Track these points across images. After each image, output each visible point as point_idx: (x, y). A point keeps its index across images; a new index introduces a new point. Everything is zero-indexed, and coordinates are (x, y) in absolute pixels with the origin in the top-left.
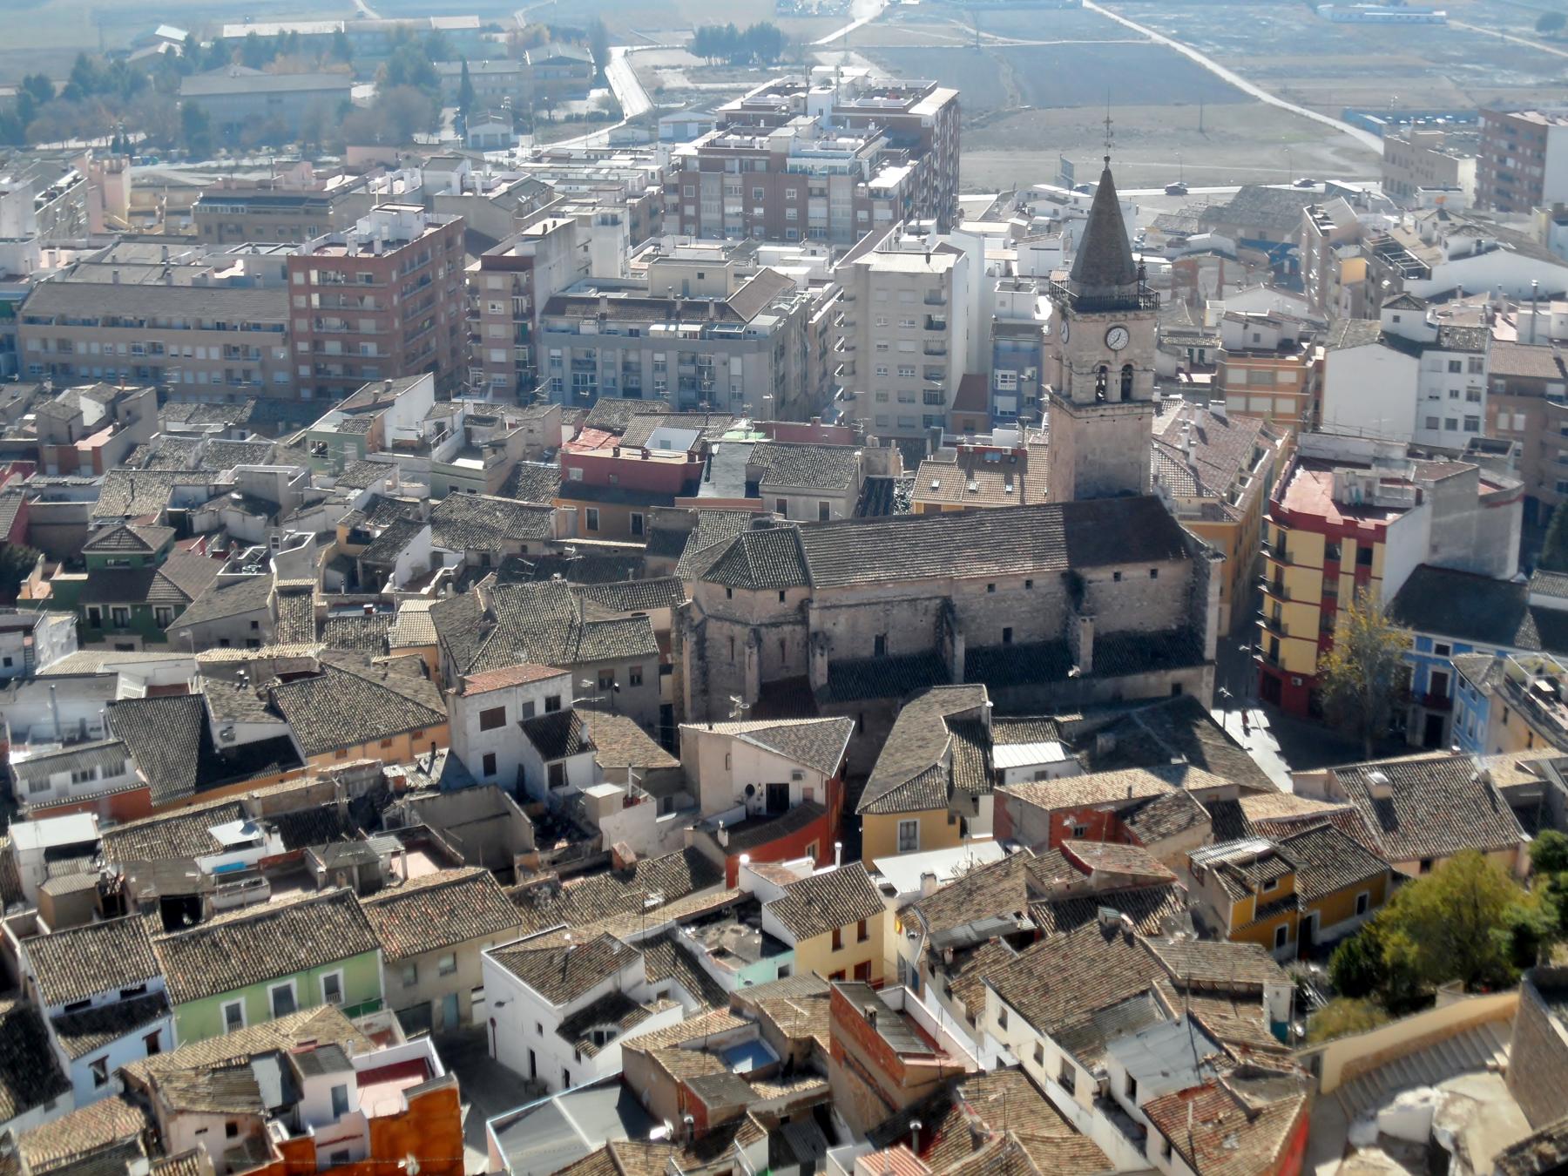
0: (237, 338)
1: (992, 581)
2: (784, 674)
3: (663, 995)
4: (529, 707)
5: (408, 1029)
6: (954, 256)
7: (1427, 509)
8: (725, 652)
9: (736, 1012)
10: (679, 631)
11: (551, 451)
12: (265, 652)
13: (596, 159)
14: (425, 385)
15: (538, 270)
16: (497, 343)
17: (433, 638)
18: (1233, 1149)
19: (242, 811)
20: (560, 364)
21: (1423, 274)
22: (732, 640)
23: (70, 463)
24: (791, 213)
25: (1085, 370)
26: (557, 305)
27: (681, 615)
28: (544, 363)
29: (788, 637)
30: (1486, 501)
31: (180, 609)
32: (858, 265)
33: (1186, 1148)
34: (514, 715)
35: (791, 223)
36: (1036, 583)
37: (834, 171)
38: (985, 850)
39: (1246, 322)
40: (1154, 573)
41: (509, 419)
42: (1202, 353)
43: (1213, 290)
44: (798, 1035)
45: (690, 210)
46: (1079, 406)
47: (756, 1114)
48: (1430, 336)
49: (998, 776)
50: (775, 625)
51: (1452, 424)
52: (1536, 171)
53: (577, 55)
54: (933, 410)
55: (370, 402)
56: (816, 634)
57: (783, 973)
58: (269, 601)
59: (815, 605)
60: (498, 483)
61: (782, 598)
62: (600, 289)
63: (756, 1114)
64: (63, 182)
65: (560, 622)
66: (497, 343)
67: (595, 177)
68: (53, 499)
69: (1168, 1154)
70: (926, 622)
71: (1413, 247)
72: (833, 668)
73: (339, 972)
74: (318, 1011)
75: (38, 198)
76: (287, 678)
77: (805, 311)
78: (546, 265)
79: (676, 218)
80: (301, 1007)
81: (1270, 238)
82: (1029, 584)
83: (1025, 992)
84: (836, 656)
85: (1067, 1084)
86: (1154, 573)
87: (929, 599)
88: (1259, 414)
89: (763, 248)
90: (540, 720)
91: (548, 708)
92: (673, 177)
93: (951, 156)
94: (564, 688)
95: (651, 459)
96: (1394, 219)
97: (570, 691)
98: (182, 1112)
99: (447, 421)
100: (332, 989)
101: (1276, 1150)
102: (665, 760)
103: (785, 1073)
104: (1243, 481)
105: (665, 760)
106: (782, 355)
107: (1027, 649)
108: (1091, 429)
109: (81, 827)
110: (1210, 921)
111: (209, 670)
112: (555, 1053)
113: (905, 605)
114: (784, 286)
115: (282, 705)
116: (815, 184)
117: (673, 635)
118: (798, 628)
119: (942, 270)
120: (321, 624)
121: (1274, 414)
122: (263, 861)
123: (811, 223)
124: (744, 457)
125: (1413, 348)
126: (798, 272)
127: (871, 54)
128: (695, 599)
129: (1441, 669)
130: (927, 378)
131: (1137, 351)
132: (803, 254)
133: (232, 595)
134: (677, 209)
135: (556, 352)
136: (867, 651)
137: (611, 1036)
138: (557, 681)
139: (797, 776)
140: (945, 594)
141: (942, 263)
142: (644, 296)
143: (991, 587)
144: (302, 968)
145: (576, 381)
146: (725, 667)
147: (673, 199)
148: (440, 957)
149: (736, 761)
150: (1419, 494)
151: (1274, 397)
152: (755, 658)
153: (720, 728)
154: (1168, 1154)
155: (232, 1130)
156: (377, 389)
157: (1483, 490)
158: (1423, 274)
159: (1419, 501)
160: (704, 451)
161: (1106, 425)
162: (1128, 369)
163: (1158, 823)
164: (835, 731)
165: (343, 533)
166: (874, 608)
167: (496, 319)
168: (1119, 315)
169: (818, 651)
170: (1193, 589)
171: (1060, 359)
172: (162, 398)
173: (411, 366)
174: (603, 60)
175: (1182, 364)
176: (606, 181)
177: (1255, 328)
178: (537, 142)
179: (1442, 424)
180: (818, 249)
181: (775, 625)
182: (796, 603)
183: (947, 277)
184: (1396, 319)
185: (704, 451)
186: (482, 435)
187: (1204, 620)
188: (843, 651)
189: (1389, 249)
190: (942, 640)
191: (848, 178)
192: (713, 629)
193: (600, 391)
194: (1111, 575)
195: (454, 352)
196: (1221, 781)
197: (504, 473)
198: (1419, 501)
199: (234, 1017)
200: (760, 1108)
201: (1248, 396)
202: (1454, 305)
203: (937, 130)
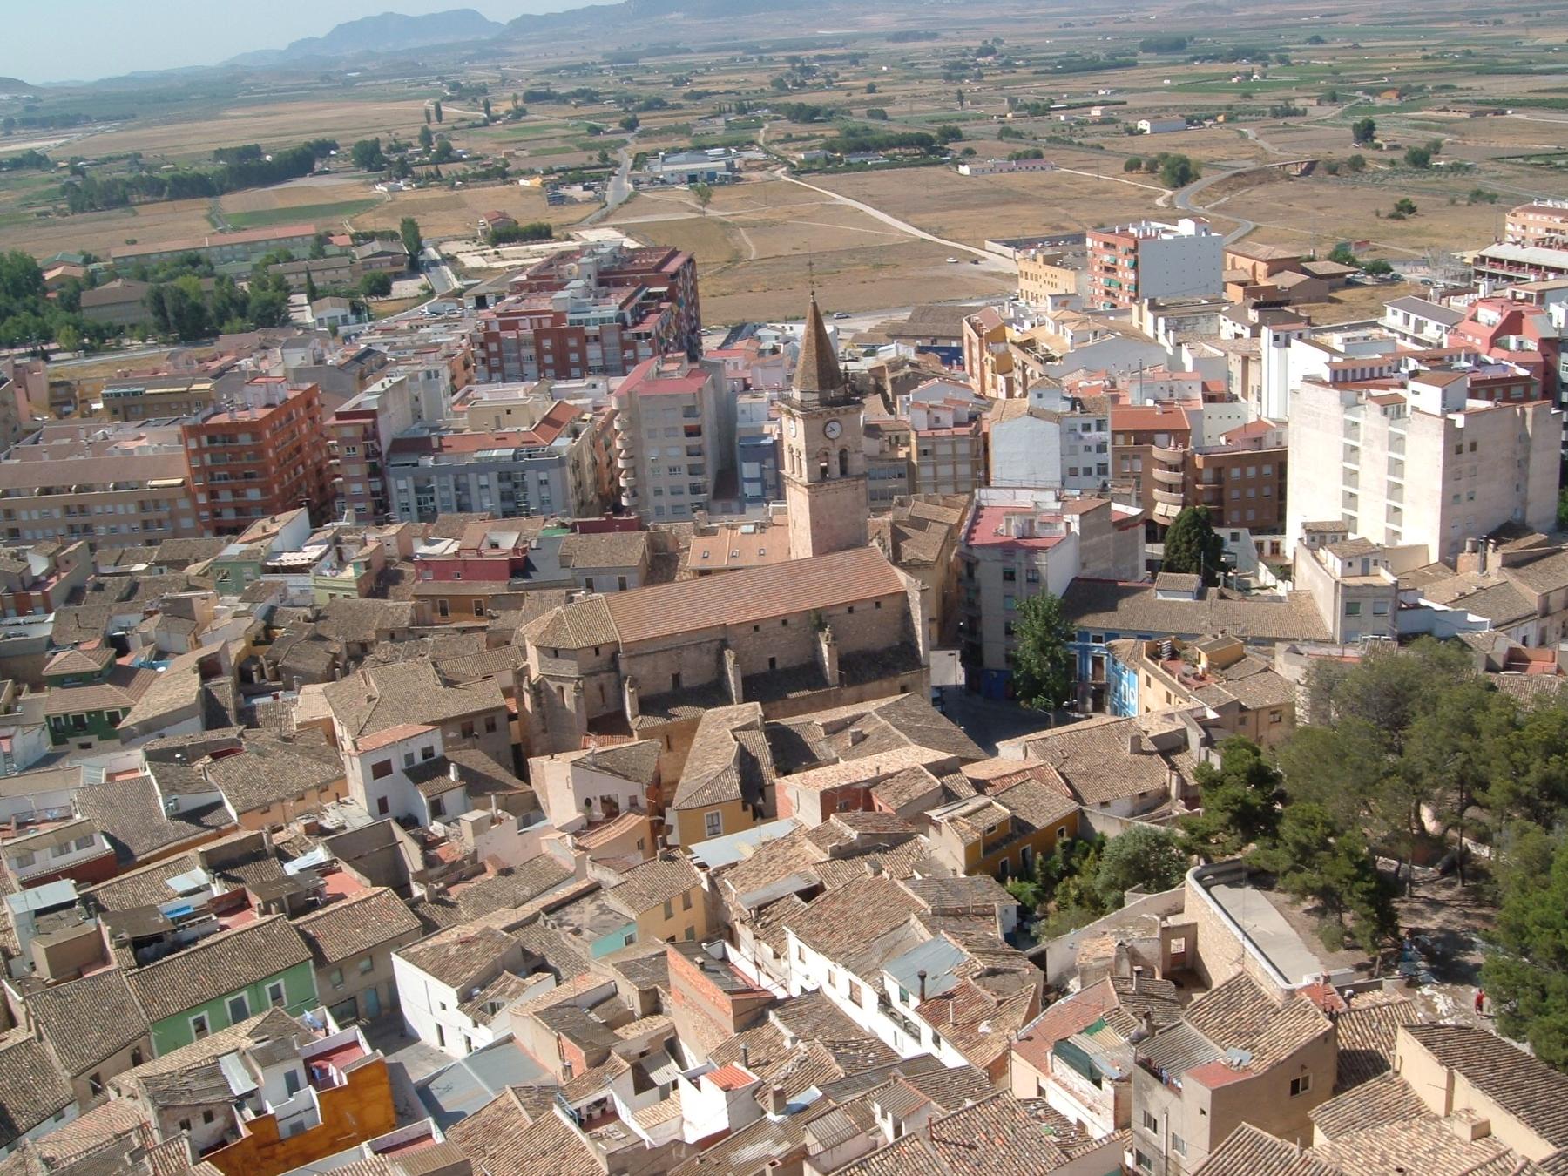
2: (605, 711)
24: (574, 357)
28: (393, 492)
31: (126, 711)
34: (398, 765)
61: (597, 652)
82: (785, 623)
90: (420, 767)
91: (425, 757)
107: (786, 671)
136: (668, 686)
143: (756, 628)
148: (361, 959)
179: (1081, 472)
195: (322, 488)
199: (201, 1028)
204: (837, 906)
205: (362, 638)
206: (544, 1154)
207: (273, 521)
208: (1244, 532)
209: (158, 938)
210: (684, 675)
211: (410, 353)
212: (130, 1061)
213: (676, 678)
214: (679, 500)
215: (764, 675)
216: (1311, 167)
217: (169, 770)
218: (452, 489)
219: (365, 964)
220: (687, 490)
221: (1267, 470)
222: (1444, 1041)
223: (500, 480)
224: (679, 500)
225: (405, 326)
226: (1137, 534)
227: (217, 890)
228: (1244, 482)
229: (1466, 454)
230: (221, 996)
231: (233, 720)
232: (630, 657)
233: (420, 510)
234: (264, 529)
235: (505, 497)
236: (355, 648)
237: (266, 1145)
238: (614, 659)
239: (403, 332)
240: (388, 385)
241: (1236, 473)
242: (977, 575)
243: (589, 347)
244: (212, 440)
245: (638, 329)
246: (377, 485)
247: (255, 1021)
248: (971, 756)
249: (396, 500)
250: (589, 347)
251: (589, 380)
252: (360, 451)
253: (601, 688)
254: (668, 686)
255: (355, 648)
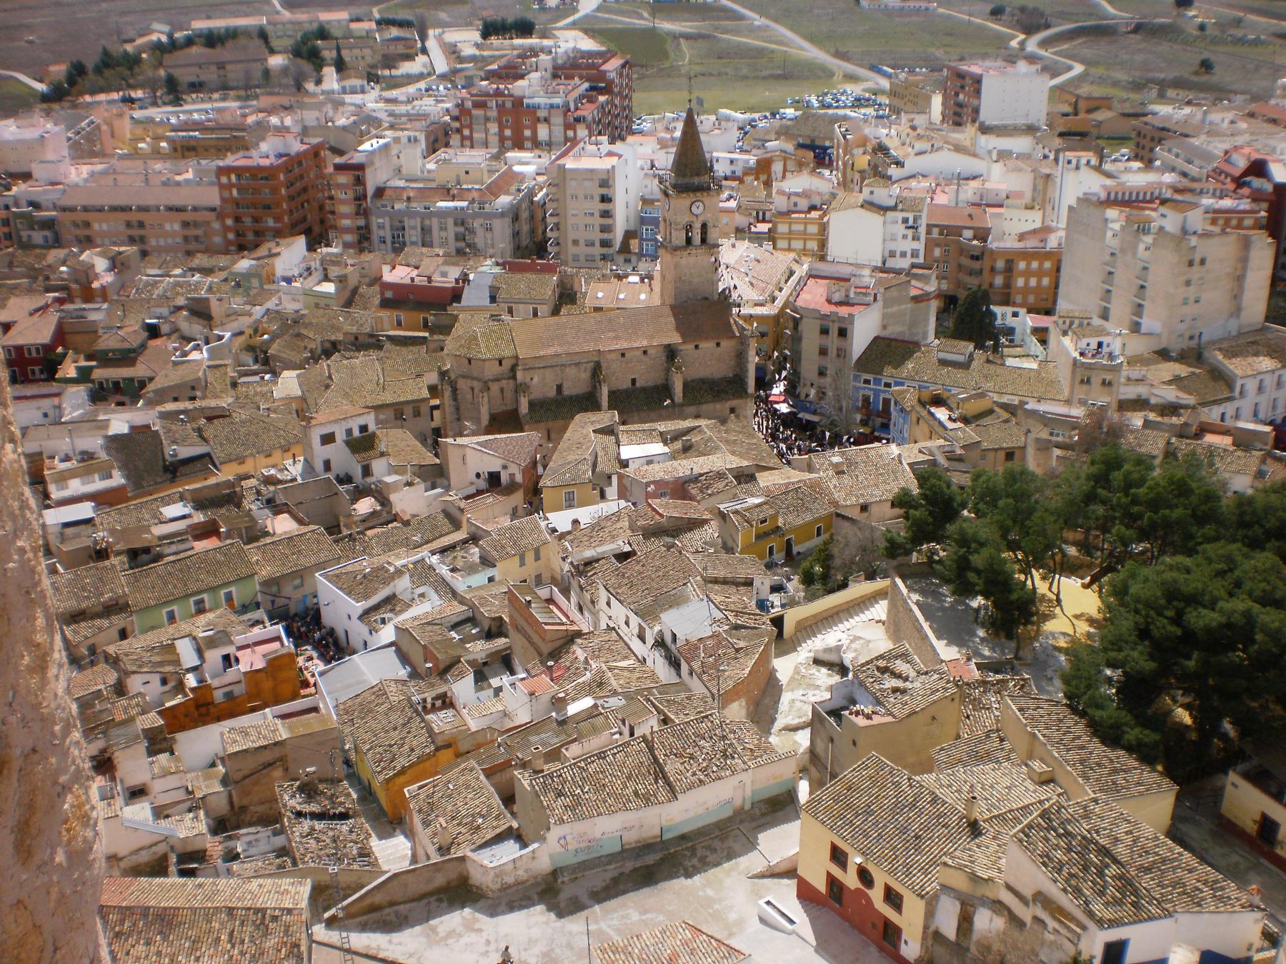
0: (188, 217)
2: (504, 408)
3: (422, 595)
4: (349, 432)
5: (271, 619)
7: (880, 304)
9: (461, 603)
11: (377, 279)
12: (198, 404)
14: (301, 242)
15: (368, 171)
16: (345, 216)
17: (300, 393)
18: (724, 671)
19: (182, 498)
21: (899, 164)
22: (473, 389)
23: (89, 295)
24: (527, 133)
26: (380, 192)
27: (443, 374)
28: (374, 228)
30: (916, 299)
31: (151, 379)
33: (699, 671)
34: (340, 437)
35: (527, 139)
38: (612, 505)
39: (789, 195)
40: (718, 345)
41: (350, 262)
43: (780, 175)
44: (493, 615)
45: (466, 132)
46: (676, 249)
47: (468, 662)
48: (891, 203)
49: (624, 464)
50: (497, 380)
51: (903, 254)
52: (975, 102)
53: (408, 36)
54: (605, 250)
55: (266, 253)
57: (491, 580)
58: (201, 374)
60: (342, 301)
61: (500, 364)
63: (468, 662)
64: (83, 124)
66: (345, 216)
68: (78, 317)
69: (691, 674)
70: (585, 375)
71: (896, 149)
73: (233, 589)
74: (218, 612)
75: (70, 135)
76: (210, 419)
77: (531, 193)
80: (210, 610)
81: (818, 143)
83: (620, 586)
84: (532, 397)
85: (642, 637)
86: (718, 345)
90: (357, 440)
91: (361, 432)
92: (456, 112)
94: (370, 420)
95: (433, 284)
96: (885, 131)
98: (134, 672)
99: (313, 264)
100: (229, 598)
101: (747, 671)
102: (430, 459)
103: (489, 635)
104: (781, 290)
105: (430, 459)
107: (644, 390)
109: (85, 510)
110: (730, 543)
111: (164, 416)
112: (358, 631)
114: (521, 177)
115: (206, 435)
119: (609, 167)
120: (234, 385)
121: (804, 249)
122: (189, 526)
124: (489, 281)
125: (883, 209)
127: (590, 32)
129: (887, 396)
133: (182, 370)
134: (458, 131)
135: (380, 221)
136: (552, 393)
137: (390, 619)
138: (365, 417)
139: (505, 467)
140: (596, 359)
141: (606, 164)
142: (433, 185)
143: (623, 355)
144: (213, 590)
147: (457, 125)
148: (294, 579)
149: (469, 459)
150: (875, 295)
151: (805, 240)
153: (460, 441)
154: (691, 674)
155: (164, 682)
156: (271, 245)
157: (914, 292)
158: (899, 164)
159: (875, 299)
160: (465, 279)
161: (692, 260)
162: (704, 226)
163: (707, 488)
164: (526, 440)
165: (249, 331)
167: (344, 202)
172: (144, 254)
173: (296, 228)
174: (423, 37)
175: (752, 220)
177: (794, 199)
178: (382, 90)
179: (898, 254)
181: (497, 380)
184: (872, 193)
185: (465, 279)
186: (334, 271)
188: (536, 394)
189: (882, 149)
191: (560, 111)
195: (322, 222)
196: (745, 463)
197: (347, 294)
198: (875, 299)
199: (172, 618)
200: (470, 657)
202: (913, 183)
203: (617, 81)
204: (638, 567)
205: (333, 338)
206: (395, 729)
208: (1022, 311)
209: (147, 550)
210: (565, 386)
211: (404, 119)
212: (117, 636)
213: (559, 388)
214: (590, 250)
215: (626, 391)
216: (1138, 29)
217: (174, 427)
219: (297, 582)
220: (597, 243)
221: (1047, 265)
222: (1035, 710)
223: (456, 224)
224: (590, 250)
225: (403, 98)
226: (928, 308)
227: (199, 517)
228: (1028, 274)
229: (1196, 268)
230: (187, 596)
231: (605, 401)
234: (270, 250)
236: (328, 345)
237: (203, 705)
238: (513, 369)
240: (376, 146)
241: (1022, 265)
242: (800, 328)
244: (239, 177)
246: (361, 222)
247: (210, 616)
248: (771, 465)
249: (376, 234)
252: (351, 195)
253: (502, 390)
254: (552, 393)
255: (328, 345)
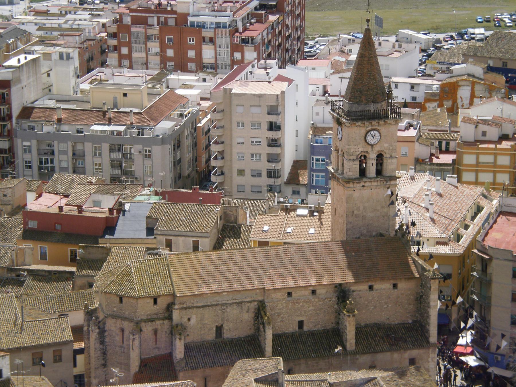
1: (290, 291)
2: (156, 353)
6: (286, 83)
8: (118, 338)
10: (89, 326)
13: (66, 13)
15: (14, 89)
20: (30, 151)
22: (123, 330)
24: (191, 54)
25: (352, 158)
27: (90, 314)
28: (19, 151)
29: (159, 327)
32: (225, 90)
36: (318, 292)
37: (218, 26)
39: (477, 123)
40: (395, 286)
42: (448, 144)
43: (466, 102)
45: (125, 51)
46: (349, 181)
54: (272, 181)
56: (177, 326)
59: (176, 307)
61: (155, 302)
62: (58, 101)
65: (7, 320)
67: (64, 26)
70: (248, 316)
72: (187, 348)
77: (195, 119)
78: (19, 86)
79: (116, 55)
82: (314, 292)
84: (189, 340)
86: (395, 286)
87: (250, 302)
88: (482, 184)
89: (172, 77)
92: (113, 29)
93: (299, 15)
95: (84, 214)
97: (9, 367)
106: (179, 146)
107: (312, 334)
108: (356, 194)
113: (235, 306)
116: (207, 33)
117: (85, 329)
118: (166, 322)
119: (278, 93)
123: (205, 61)
124: (146, 212)
126: (193, 93)
128: (100, 305)
130: (269, 161)
131: (386, 145)
132: (197, 81)
134: (116, 49)
140: (261, 298)
141: (276, 89)
142: (88, 107)
143: (289, 294)
145: (41, 162)
146: (118, 349)
147: (114, 42)
151: (495, 172)
152: (137, 343)
160: (120, 209)
161: (366, 193)
162: (380, 157)
166: (214, 308)
168: (374, 123)
169: (178, 336)
170: (421, 297)
171: (337, 151)
175: (434, 151)
176: (72, 29)
177: (482, 127)
180: (208, 78)
182: (165, 306)
183: (280, 98)
185: (120, 209)
187: (428, 317)
188: (193, 337)
190: (258, 329)
192: (112, 325)
193: (57, 169)
194: (367, 287)
201: (477, 172)
207: (61, 209)
210: (226, 327)
214: (256, 181)
218: (70, 154)
220: (264, 174)
223: (111, 150)
224: (256, 181)
232: (182, 309)
233: (40, 168)
235: (114, 164)
238: (169, 308)
239: (53, 15)
240: (23, 61)
242: (489, 270)
243: (204, 47)
245: (247, 34)
250: (204, 47)
251: (202, 75)
253: (156, 332)
254: (211, 336)
